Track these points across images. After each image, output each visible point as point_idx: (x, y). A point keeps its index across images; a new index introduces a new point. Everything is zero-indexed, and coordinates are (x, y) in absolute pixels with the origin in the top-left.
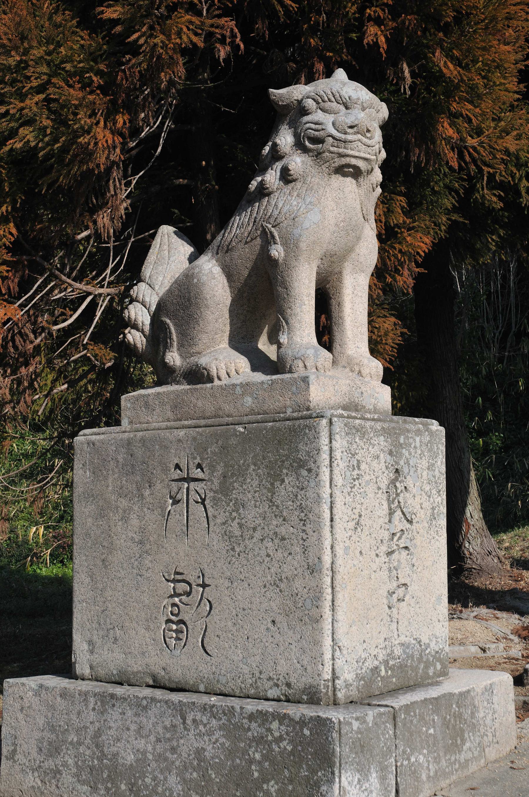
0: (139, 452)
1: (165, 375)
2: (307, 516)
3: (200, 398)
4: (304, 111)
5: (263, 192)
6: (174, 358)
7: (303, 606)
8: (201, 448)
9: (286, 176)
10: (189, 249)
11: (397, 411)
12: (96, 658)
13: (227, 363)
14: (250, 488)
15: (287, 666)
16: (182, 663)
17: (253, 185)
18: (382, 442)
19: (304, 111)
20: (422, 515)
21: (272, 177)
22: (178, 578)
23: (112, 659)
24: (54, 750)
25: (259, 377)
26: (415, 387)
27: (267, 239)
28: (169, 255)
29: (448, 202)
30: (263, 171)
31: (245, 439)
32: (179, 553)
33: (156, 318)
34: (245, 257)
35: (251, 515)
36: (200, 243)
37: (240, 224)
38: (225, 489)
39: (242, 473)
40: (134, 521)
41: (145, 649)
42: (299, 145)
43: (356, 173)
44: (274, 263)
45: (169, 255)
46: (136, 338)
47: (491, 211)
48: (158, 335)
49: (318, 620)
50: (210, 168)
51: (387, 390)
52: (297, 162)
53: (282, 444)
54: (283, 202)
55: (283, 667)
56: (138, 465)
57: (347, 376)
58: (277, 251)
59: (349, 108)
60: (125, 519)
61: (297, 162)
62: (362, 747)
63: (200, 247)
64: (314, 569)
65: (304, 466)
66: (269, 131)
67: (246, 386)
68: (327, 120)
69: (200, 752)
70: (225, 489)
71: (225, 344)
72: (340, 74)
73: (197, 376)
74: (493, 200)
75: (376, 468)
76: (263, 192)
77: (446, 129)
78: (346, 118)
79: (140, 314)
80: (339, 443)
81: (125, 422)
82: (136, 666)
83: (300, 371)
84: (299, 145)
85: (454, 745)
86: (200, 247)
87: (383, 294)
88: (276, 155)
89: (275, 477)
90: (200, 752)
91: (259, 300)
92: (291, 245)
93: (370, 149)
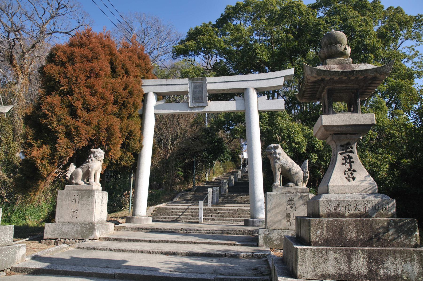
0: (69, 193)
1: (72, 183)
2: (92, 202)
3: (77, 187)
4: (95, 153)
5: (88, 162)
6: (74, 181)
7: (91, 213)
8: (78, 193)
9: (92, 160)
10: (75, 167)
11: (102, 190)
12: (59, 220)
13: (82, 183)
14: (85, 198)
15: (88, 220)
16: (74, 220)
17: (87, 160)
18: (101, 194)
19: (95, 153)
20: (105, 203)
21: (90, 160)
22: (73, 209)
23: (62, 220)
24: (54, 231)
25: (86, 185)
26: (105, 188)
27: (89, 168)
28: (72, 168)
29: (108, 162)
30: (89, 159)
31: (85, 192)
32: (74, 206)
33: (71, 176)
34: (85, 170)
35: (85, 202)
36: (78, 166)
37: (85, 165)
38: (81, 198)
39: (84, 197)
40: (67, 202)
41: (68, 218)
42: (94, 157)
43: (101, 161)
44: (89, 171)
45: (72, 168)
46: (68, 178)
47: (114, 163)
48: (71, 178)
49: (93, 214)
50: (81, 158)
51: (101, 188)
52: (94, 159)
53: (90, 193)
54: (91, 163)
55: (88, 220)
56: (68, 195)
57: (96, 185)
58: (90, 170)
59: (100, 153)
60: (66, 202)
61: (94, 159)
62: (98, 228)
63: (77, 167)
64: (93, 208)
65: (93, 196)
66: (90, 154)
67: (84, 186)
68: (98, 154)
69: (77, 230)
70: (81, 198)
71: (81, 180)
72: (100, 148)
73: (77, 184)
74: (114, 162)
75: (101, 197)
76: (88, 162)
77: (110, 154)
78: (100, 155)
79: (69, 175)
80: (97, 194)
81: (65, 189)
82: (66, 221)
83: (92, 184)
84: (94, 157)
85: (107, 230)
86: (77, 167)
87: (101, 175)
88: (91, 157)
89: (89, 197)
90: (77, 230)
91: (87, 175)
92: (92, 169)
93: (102, 158)
